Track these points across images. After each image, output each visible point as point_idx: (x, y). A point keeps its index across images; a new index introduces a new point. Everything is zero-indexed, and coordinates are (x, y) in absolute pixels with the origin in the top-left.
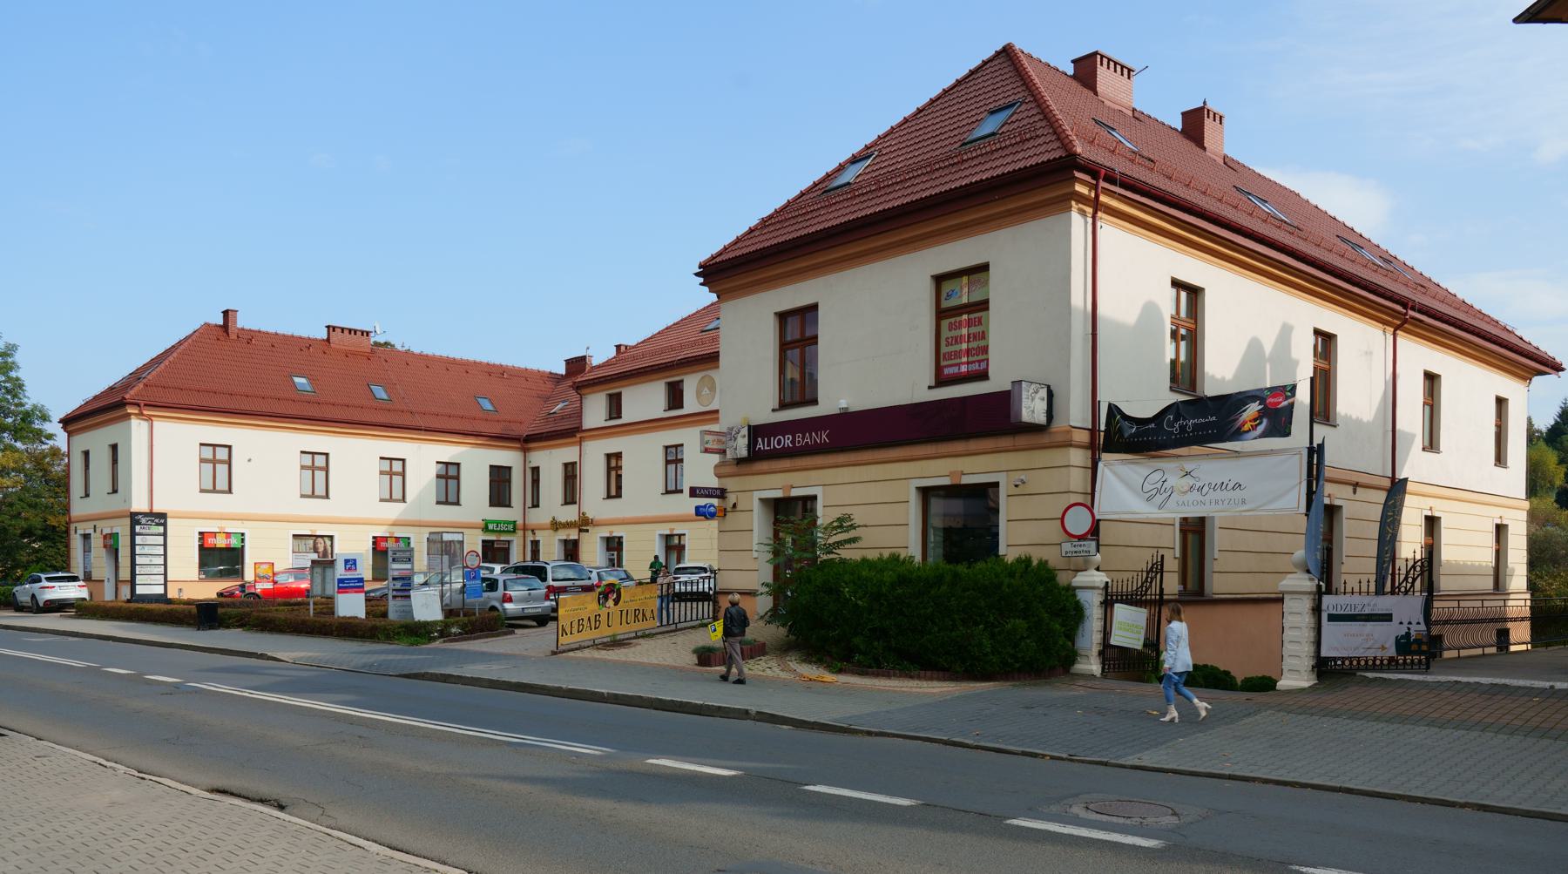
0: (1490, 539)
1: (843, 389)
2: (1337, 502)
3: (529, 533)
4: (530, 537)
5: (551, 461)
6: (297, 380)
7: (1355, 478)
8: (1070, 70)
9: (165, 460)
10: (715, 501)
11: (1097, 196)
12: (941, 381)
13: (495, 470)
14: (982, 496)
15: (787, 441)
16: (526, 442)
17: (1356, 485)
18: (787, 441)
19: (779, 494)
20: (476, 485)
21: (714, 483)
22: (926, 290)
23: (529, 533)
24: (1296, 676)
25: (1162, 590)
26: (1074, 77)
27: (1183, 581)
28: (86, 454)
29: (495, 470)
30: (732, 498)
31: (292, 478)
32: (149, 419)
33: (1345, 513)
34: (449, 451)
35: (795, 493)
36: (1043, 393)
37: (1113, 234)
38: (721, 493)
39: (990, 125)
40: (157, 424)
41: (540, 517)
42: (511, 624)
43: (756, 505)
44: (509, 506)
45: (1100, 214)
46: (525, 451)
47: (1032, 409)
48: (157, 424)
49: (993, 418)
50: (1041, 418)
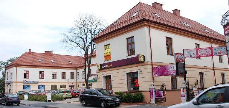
0: (221, 77)
1: (114, 58)
2: (203, 72)
3: (77, 83)
4: (77, 84)
5: (81, 71)
6: (52, 61)
7: (206, 68)
8: (152, 5)
9: (17, 75)
10: (96, 77)
11: (149, 25)
12: (129, 55)
13: (71, 73)
14: (65, 73)
15: (106, 66)
16: (77, 68)
17: (206, 69)
18: (106, 66)
19: (106, 75)
20: (68, 76)
21: (96, 74)
22: (125, 41)
23: (77, 83)
24: (49, 97)
25: (165, 88)
26: (152, 6)
27: (201, 86)
28: (8, 73)
29: (71, 73)
30: (99, 76)
31: (51, 76)
32: (16, 67)
33: (204, 74)
34: (64, 71)
35: (108, 75)
36: (143, 56)
37: (153, 31)
38: (97, 75)
39: (135, 14)
40: (17, 68)
41: (78, 81)
42: (65, 99)
43: (102, 77)
44: (65, 79)
45: (150, 27)
46: (77, 70)
47: (141, 59)
48: (17, 68)
49: (135, 61)
50: (143, 61)
